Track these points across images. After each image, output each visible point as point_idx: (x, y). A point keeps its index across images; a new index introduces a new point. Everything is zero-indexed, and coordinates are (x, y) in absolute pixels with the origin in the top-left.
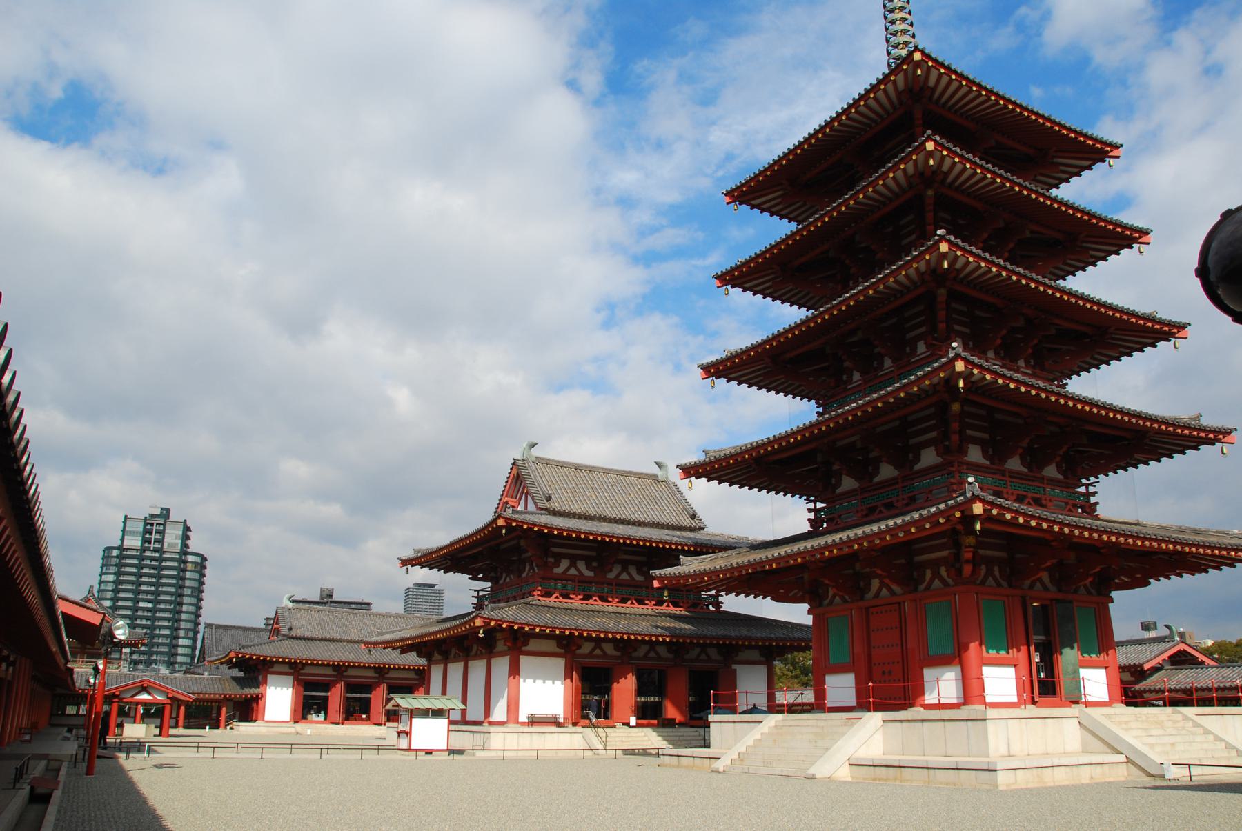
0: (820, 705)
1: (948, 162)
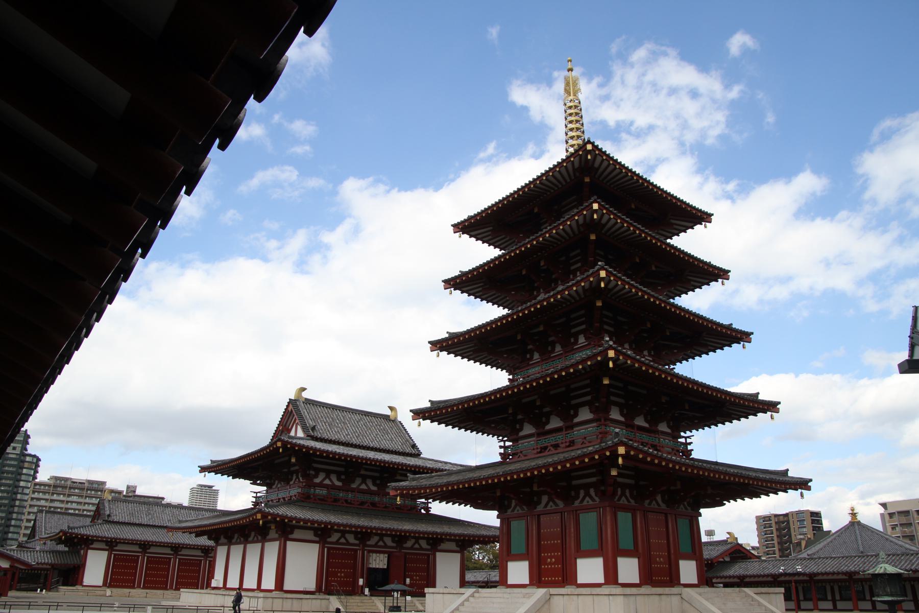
0: (503, 582)
1: (606, 218)
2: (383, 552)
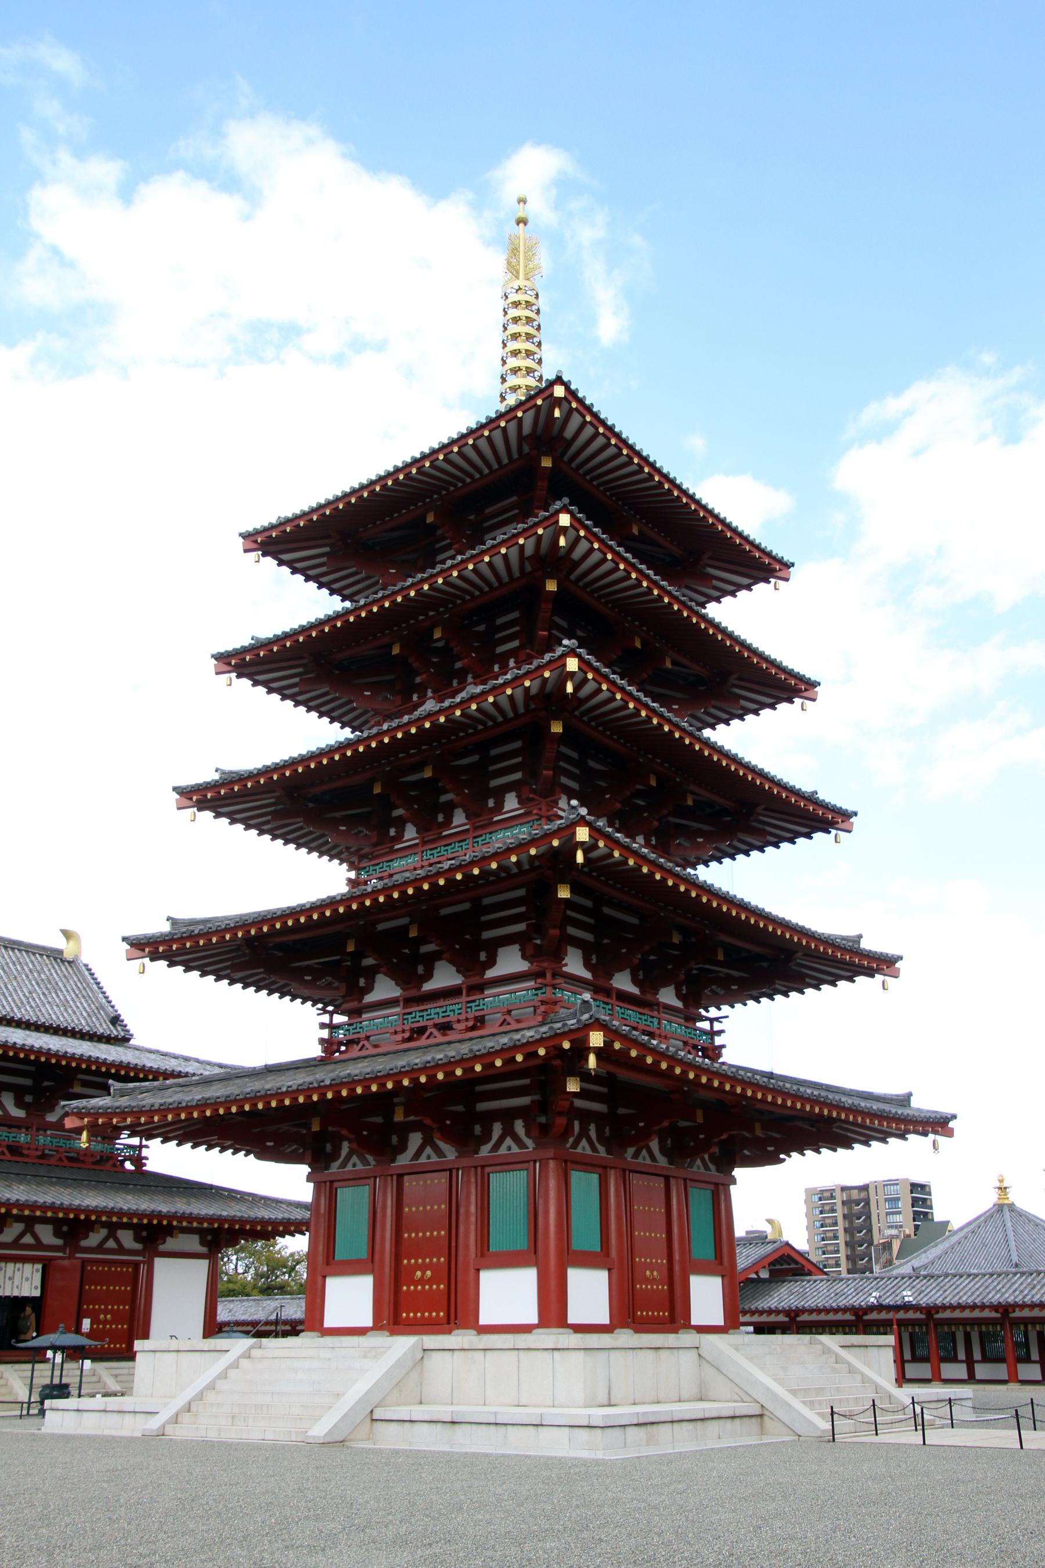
0: (311, 1322)
1: (583, 546)
2: (32, 1260)
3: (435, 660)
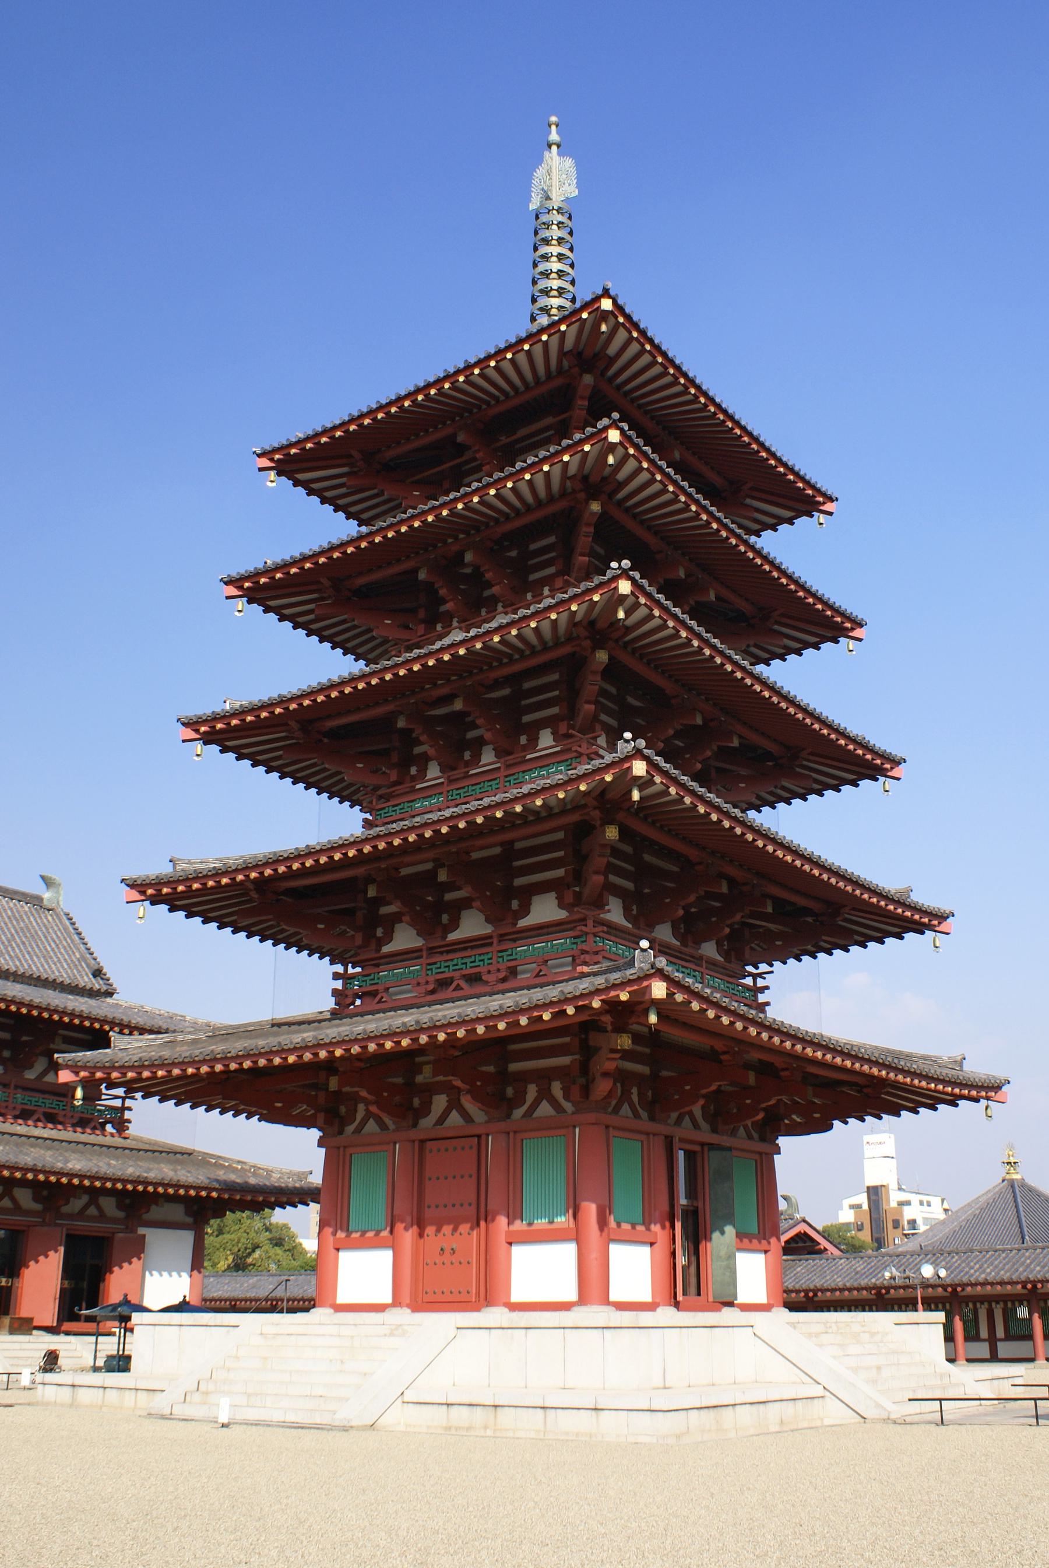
1: (631, 465)
3: (462, 587)
